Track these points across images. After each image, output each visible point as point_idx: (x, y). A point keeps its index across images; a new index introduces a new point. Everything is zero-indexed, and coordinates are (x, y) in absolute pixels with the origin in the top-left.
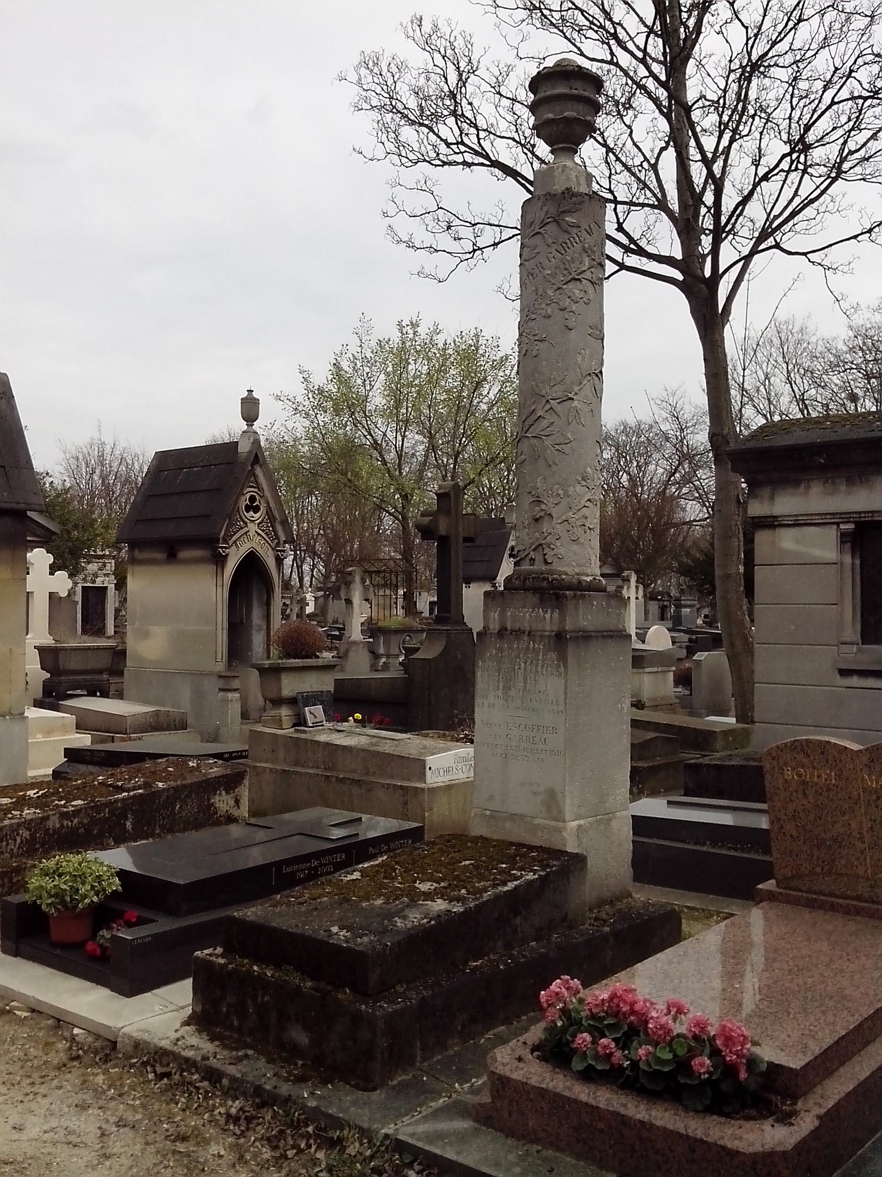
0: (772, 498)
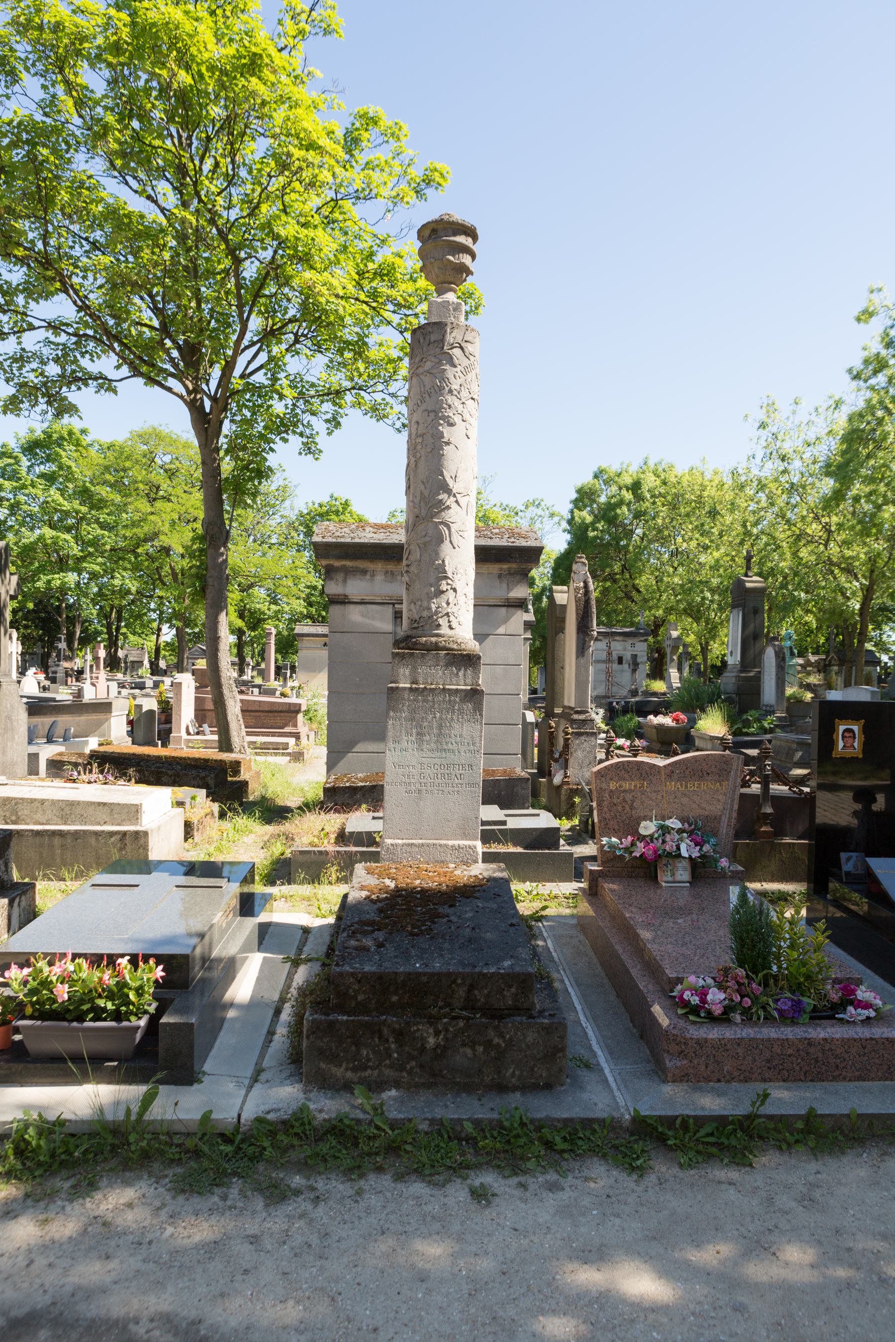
0: (345, 581)
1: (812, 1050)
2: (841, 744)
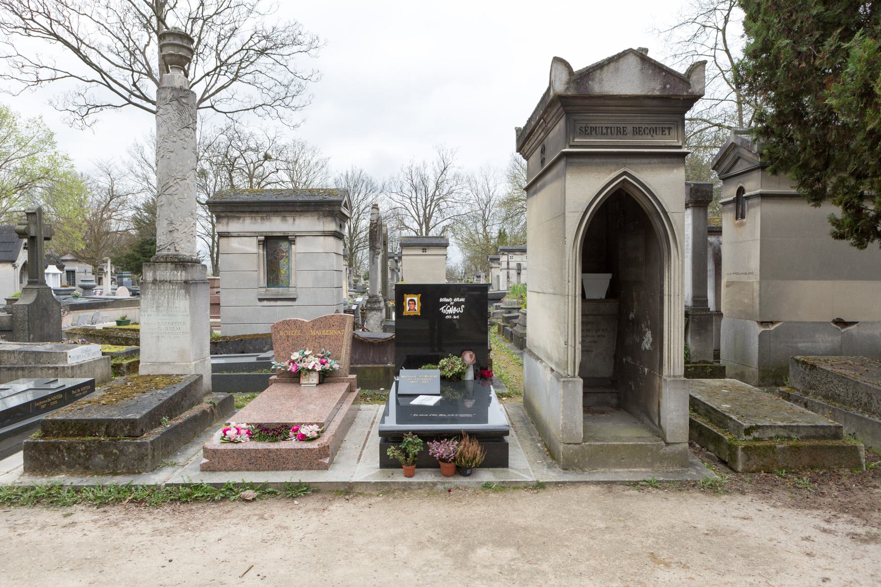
0: (228, 224)
1: (271, 455)
2: (408, 308)
